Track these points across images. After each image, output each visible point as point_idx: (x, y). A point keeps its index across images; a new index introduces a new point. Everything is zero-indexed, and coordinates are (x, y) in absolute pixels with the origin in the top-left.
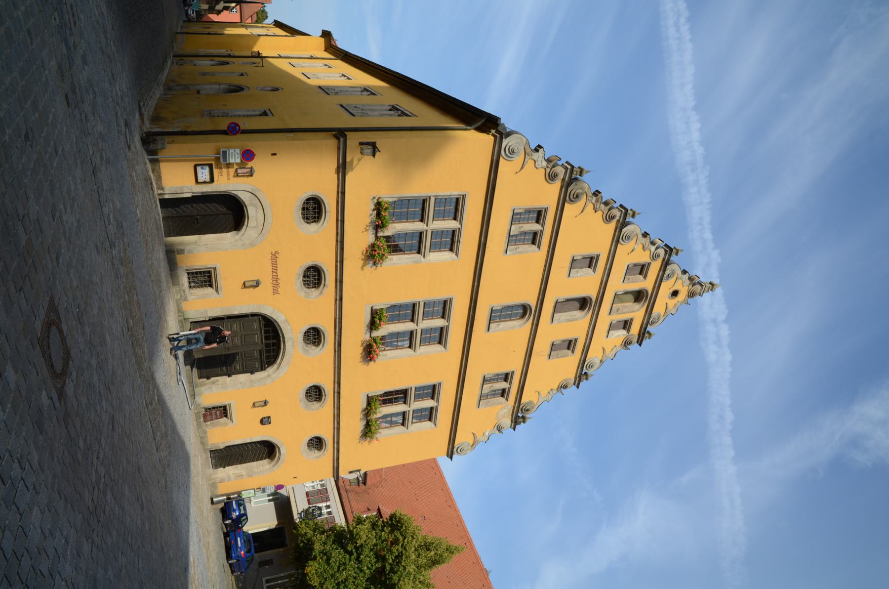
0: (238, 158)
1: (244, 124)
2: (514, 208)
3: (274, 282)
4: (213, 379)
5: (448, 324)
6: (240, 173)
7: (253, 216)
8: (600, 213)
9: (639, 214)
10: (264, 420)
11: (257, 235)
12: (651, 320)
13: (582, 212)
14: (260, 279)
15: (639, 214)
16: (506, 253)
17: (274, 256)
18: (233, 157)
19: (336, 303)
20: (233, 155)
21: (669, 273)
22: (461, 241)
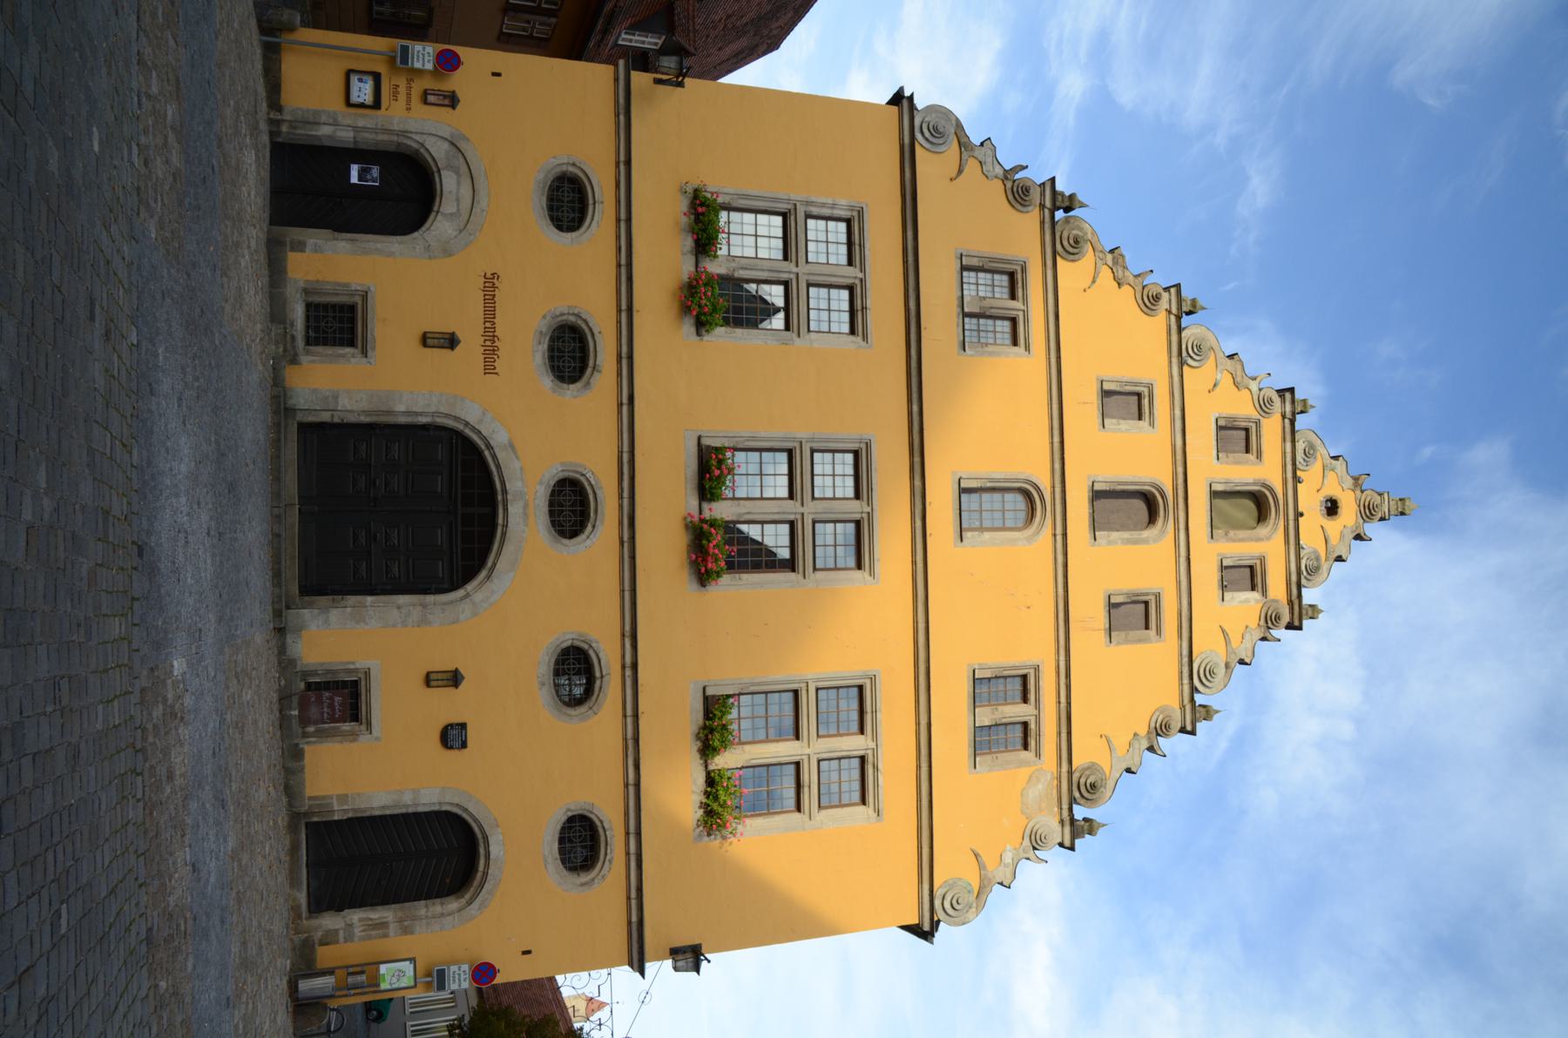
3: (488, 343)
5: (869, 510)
7: (450, 192)
11: (455, 233)
12: (1303, 562)
14: (458, 333)
17: (490, 283)
19: (620, 412)
20: (457, 977)
21: (1304, 446)
22: (868, 306)
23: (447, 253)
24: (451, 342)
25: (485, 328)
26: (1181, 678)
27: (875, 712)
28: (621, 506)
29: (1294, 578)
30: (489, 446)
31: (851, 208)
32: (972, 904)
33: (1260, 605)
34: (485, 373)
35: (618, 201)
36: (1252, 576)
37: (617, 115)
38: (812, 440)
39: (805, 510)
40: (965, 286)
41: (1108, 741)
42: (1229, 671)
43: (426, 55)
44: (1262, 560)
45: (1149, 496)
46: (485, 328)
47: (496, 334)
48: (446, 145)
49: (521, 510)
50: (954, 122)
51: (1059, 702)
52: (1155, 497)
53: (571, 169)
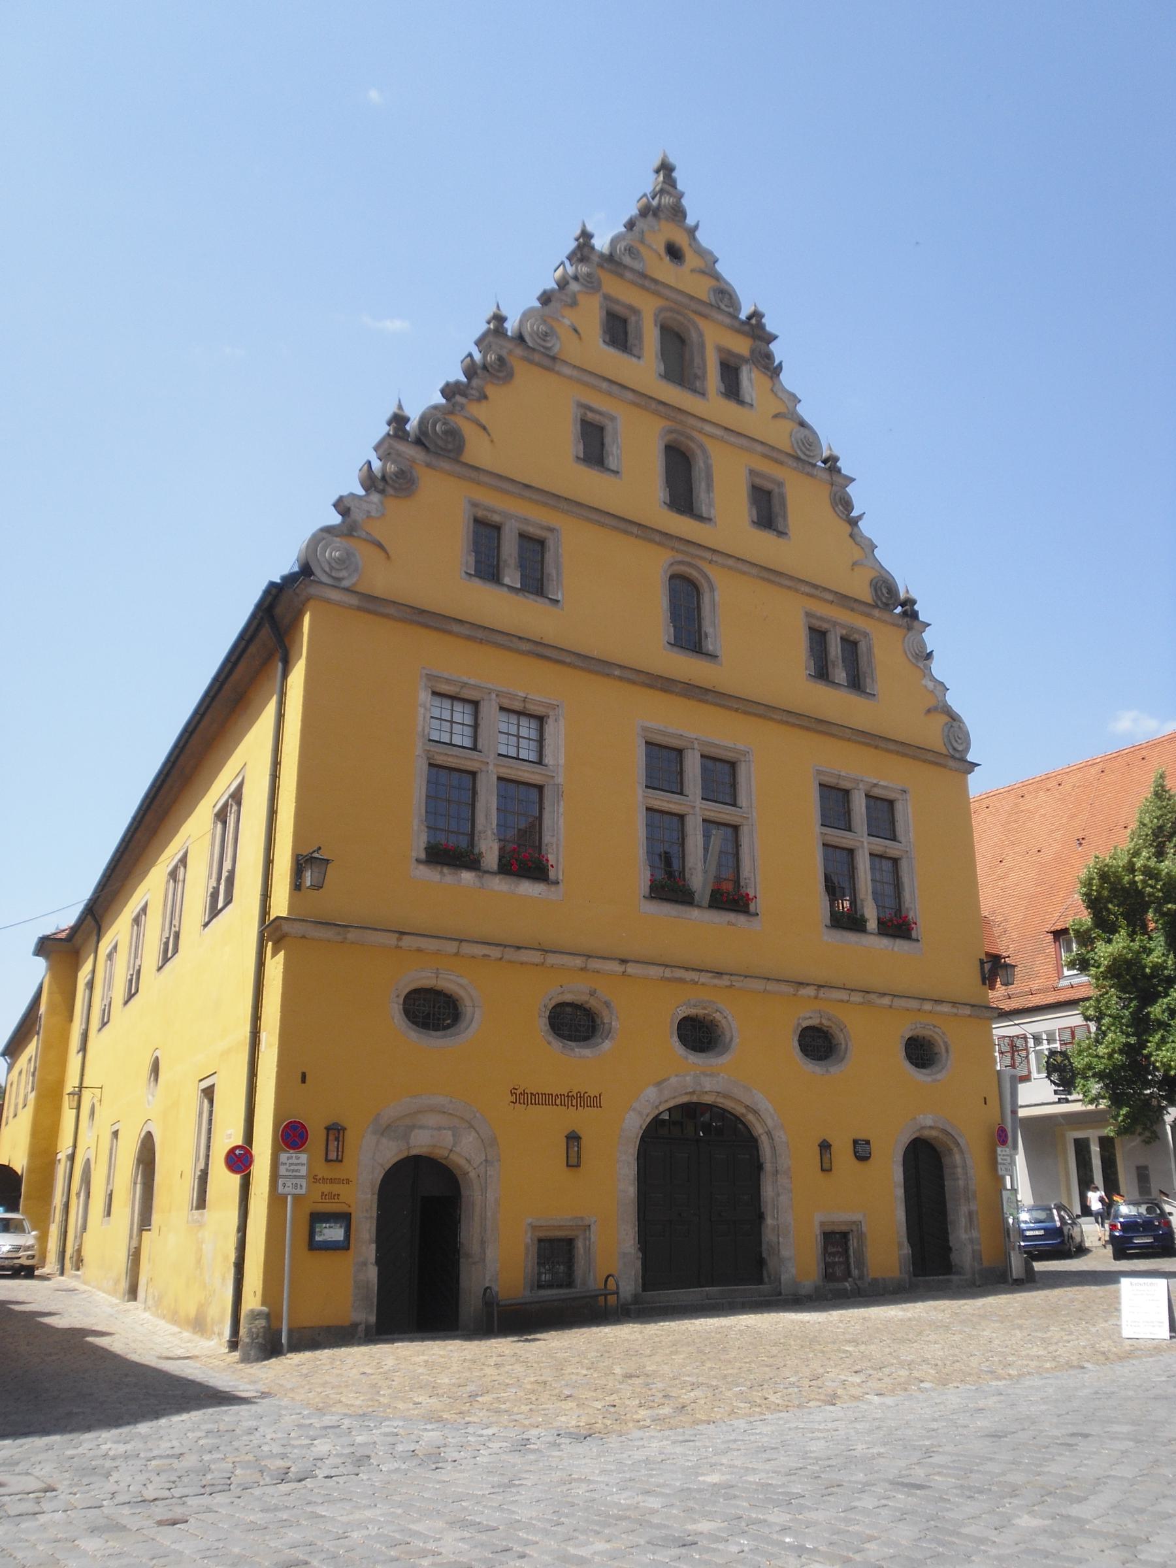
0: (298, 1158)
1: (230, 1136)
2: (463, 574)
4: (764, 1255)
6: (338, 1155)
8: (490, 390)
9: (498, 307)
10: (861, 1153)
11: (473, 1134)
13: (484, 428)
15: (498, 307)
16: (558, 601)
17: (521, 1097)
18: (296, 1168)
20: (292, 1167)
24: (573, 1138)
25: (561, 1105)
34: (601, 1107)
43: (290, 1161)
46: (561, 1105)
47: (530, 1105)
50: (325, 535)
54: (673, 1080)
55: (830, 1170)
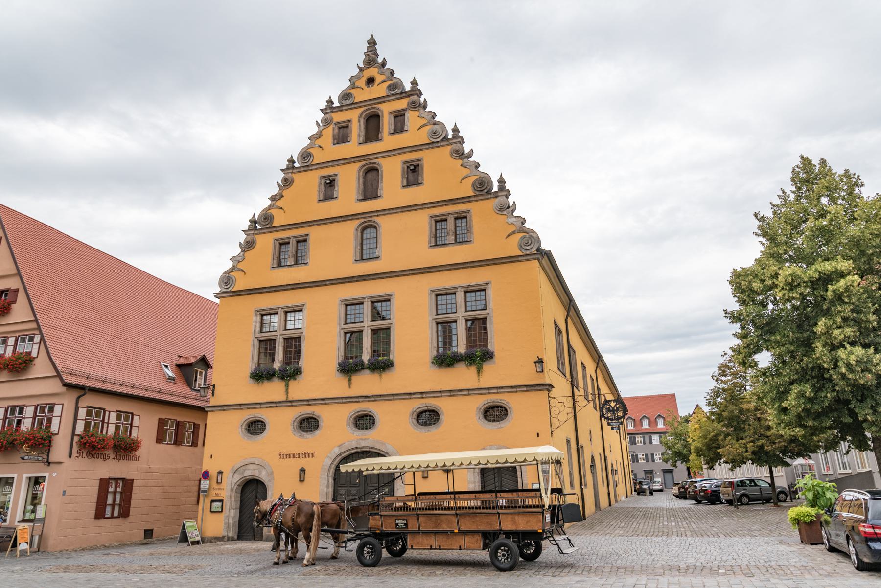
5: (366, 298)
17: (283, 456)
19: (328, 404)
23: (272, 473)
24: (303, 470)
26: (439, 147)
27: (446, 289)
28: (362, 401)
29: (398, 96)
30: (340, 455)
31: (256, 315)
32: (530, 235)
33: (410, 111)
35: (254, 408)
36: (399, 116)
37: (224, 410)
38: (340, 324)
39: (366, 326)
40: (464, 240)
41: (463, 179)
42: (437, 123)
44: (391, 113)
45: (366, 171)
48: (236, 475)
49: (363, 441)
51: (445, 205)
52: (365, 169)
53: (244, 427)
54: (346, 444)
55: (221, 483)
